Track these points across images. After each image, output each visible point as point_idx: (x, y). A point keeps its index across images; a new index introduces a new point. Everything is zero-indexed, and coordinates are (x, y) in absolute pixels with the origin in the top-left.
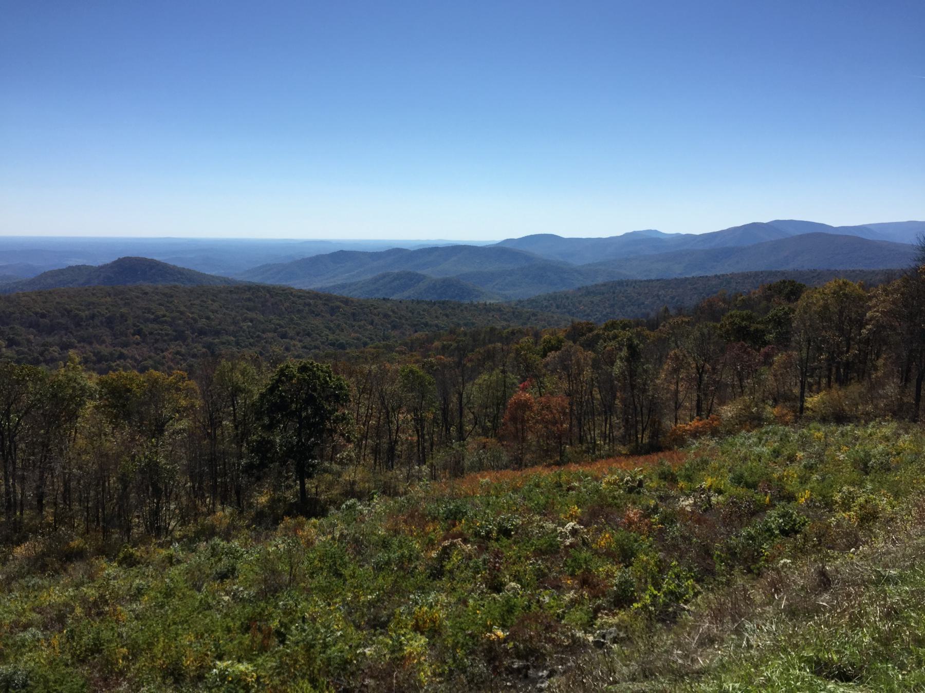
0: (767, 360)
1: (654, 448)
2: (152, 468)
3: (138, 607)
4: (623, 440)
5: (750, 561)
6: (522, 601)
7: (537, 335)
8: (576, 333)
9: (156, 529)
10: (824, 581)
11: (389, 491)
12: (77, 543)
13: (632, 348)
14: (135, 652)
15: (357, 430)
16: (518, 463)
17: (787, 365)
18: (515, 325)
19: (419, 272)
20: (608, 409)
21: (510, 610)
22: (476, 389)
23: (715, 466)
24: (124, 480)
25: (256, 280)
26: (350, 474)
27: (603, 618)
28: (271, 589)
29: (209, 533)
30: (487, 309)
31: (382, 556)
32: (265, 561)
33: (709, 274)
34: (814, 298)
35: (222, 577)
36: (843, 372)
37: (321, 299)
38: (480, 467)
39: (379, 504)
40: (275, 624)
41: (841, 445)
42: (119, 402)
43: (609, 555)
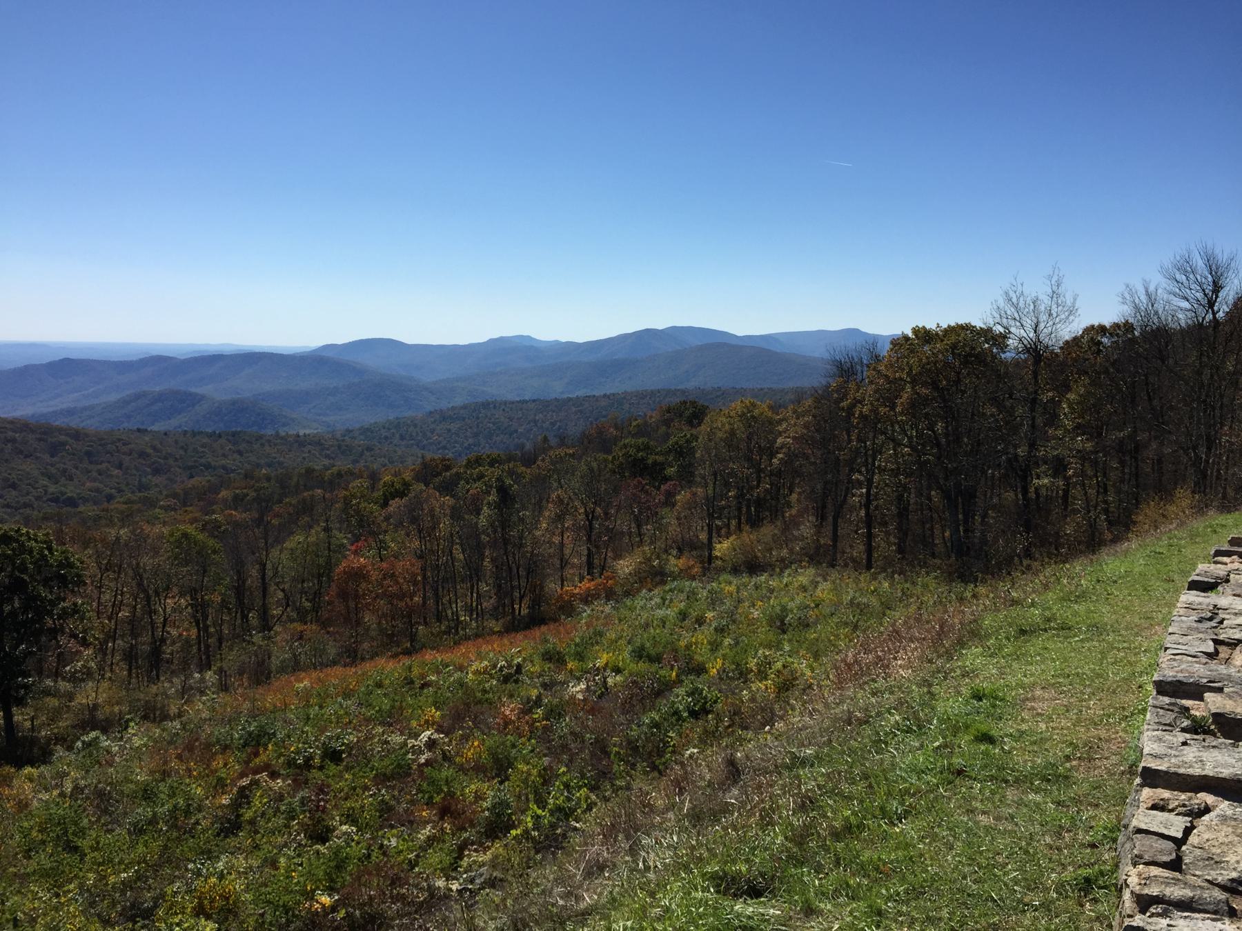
0: (669, 502)
1: (536, 620)
4: (496, 614)
5: (653, 756)
6: (357, 851)
7: (374, 477)
8: (427, 473)
10: (734, 771)
11: (153, 714)
13: (503, 491)
15: (96, 627)
16: (352, 656)
17: (691, 505)
18: (342, 464)
19: (193, 390)
22: (288, 554)
23: (610, 639)
26: (88, 694)
30: (300, 442)
31: (143, 812)
33: (596, 393)
34: (719, 422)
36: (757, 510)
37: (33, 431)
38: (295, 667)
39: (137, 736)
41: (758, 599)
43: (479, 769)
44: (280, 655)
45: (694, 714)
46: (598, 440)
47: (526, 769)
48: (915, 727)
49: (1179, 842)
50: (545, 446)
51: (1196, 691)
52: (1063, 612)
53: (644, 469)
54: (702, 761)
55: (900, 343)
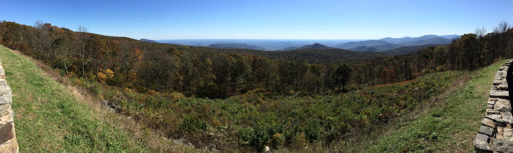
0: (430, 61)
1: (411, 79)
2: (318, 82)
3: (315, 105)
4: (405, 77)
5: (427, 98)
6: (385, 109)
7: (388, 58)
8: (395, 57)
9: (318, 92)
10: (437, 100)
11: (360, 89)
12: (306, 93)
13: (406, 60)
14: (314, 113)
15: (354, 77)
16: (385, 83)
17: (433, 62)
18: (384, 56)
20: (402, 72)
21: (383, 110)
22: (376, 69)
23: (422, 81)
24: (313, 83)
25: (336, 47)
26: (353, 85)
27: (402, 111)
28: (338, 105)
29: (327, 94)
30: (378, 53)
31: (358, 101)
32: (337, 101)
34: (436, 49)
35: (329, 102)
36: (442, 62)
38: (377, 84)
39: (358, 91)
40: (338, 111)
41: (443, 75)
42: (313, 70)
43: (402, 99)
44: (376, 82)
45: (434, 92)
46: (419, 53)
47: (410, 99)
48: (462, 92)
49: (493, 105)
50: (411, 53)
51: (498, 84)
52: (483, 75)
53: (426, 57)
54: (433, 98)
55: (462, 37)
